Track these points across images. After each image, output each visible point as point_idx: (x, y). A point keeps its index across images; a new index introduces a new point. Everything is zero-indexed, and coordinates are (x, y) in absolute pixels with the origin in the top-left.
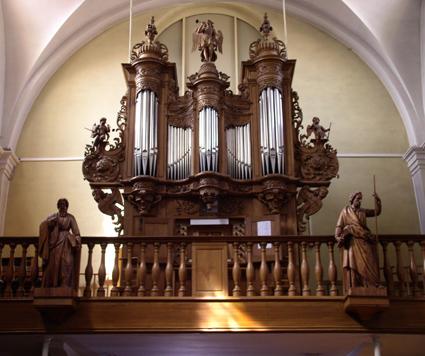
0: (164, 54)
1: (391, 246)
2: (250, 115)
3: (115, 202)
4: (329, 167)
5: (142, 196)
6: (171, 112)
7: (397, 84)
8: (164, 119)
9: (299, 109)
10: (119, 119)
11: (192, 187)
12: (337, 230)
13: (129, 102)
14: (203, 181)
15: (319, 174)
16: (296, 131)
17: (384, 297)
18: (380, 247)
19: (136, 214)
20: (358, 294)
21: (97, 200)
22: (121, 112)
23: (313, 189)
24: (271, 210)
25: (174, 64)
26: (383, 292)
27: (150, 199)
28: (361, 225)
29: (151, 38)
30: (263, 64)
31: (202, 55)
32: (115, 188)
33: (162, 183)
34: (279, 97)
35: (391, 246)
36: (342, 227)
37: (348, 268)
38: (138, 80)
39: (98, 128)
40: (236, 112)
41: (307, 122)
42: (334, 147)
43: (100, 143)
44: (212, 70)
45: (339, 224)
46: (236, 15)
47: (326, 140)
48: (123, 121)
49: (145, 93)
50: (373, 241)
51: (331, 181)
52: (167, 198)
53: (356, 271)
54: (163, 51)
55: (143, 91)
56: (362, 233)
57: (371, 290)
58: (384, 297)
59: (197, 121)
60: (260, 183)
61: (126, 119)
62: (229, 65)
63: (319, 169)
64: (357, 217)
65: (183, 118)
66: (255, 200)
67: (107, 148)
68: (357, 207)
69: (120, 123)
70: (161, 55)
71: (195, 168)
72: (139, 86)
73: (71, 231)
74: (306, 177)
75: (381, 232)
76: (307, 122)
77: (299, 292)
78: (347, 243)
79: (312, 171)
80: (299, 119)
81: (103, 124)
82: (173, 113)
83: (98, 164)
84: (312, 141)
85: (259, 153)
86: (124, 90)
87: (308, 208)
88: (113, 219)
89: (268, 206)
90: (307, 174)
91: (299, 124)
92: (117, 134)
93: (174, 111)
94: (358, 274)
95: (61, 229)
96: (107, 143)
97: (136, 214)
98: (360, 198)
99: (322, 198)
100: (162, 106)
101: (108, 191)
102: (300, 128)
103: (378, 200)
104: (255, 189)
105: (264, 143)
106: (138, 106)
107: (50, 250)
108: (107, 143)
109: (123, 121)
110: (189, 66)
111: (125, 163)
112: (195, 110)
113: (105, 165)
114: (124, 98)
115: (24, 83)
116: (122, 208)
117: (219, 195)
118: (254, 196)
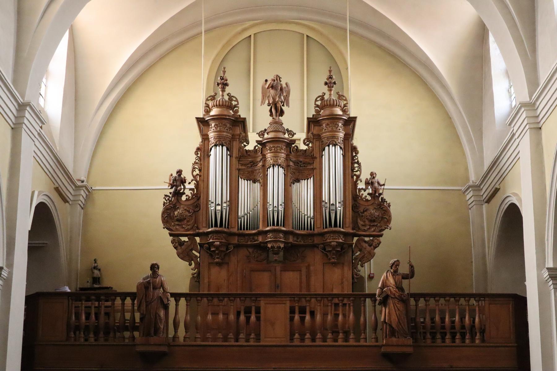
0: (235, 106)
2: (313, 169)
3: (192, 250)
4: (382, 218)
5: (217, 247)
6: (242, 165)
8: (235, 173)
9: (358, 163)
10: (194, 169)
11: (260, 239)
12: (378, 292)
13: (203, 153)
14: (270, 235)
15: (374, 226)
16: (355, 184)
17: (410, 346)
19: (211, 261)
21: (175, 248)
22: (195, 163)
23: (367, 239)
24: (330, 259)
25: (245, 119)
26: (410, 341)
27: (223, 249)
28: (397, 288)
29: (223, 90)
30: (327, 121)
31: (271, 111)
32: (191, 237)
33: (234, 234)
34: (339, 152)
36: (382, 288)
38: (212, 135)
39: (175, 180)
40: (303, 166)
41: (365, 175)
42: (388, 200)
43: (178, 194)
44: (277, 125)
45: (380, 285)
46: (306, 32)
47: (380, 194)
48: (197, 172)
49: (218, 147)
51: (384, 232)
52: (238, 246)
53: (390, 326)
54: (234, 103)
55: (216, 145)
56: (397, 294)
58: (410, 346)
59: (265, 176)
60: (322, 235)
61: (200, 170)
62: (296, 122)
63: (374, 221)
64: (394, 279)
65: (253, 172)
66: (316, 249)
67: (184, 198)
69: (195, 173)
70: (231, 107)
71: (263, 221)
72: (212, 141)
73: (161, 289)
74: (363, 228)
75: (412, 291)
76: (365, 175)
77: (324, 339)
78: (384, 302)
79: (367, 222)
80: (358, 173)
81: (180, 175)
82: (247, 166)
83: (176, 213)
84: (368, 194)
85: (321, 208)
86: (197, 141)
87: (363, 257)
88: (190, 265)
89: (327, 256)
90: (363, 225)
91: (358, 177)
92: (192, 186)
93: (245, 165)
95: (155, 288)
96: (184, 193)
97: (211, 261)
98: (398, 265)
99: (375, 248)
100: (234, 159)
101: (185, 239)
102: (359, 182)
103: (412, 267)
104: (317, 240)
105: (325, 197)
106: (212, 158)
107: (147, 306)
108: (184, 193)
109: (197, 172)
110: (258, 121)
111: (201, 211)
112: (263, 166)
113: (183, 210)
114: (198, 149)
115: (202, 188)
116: (198, 254)
117: (285, 247)
118: (314, 246)
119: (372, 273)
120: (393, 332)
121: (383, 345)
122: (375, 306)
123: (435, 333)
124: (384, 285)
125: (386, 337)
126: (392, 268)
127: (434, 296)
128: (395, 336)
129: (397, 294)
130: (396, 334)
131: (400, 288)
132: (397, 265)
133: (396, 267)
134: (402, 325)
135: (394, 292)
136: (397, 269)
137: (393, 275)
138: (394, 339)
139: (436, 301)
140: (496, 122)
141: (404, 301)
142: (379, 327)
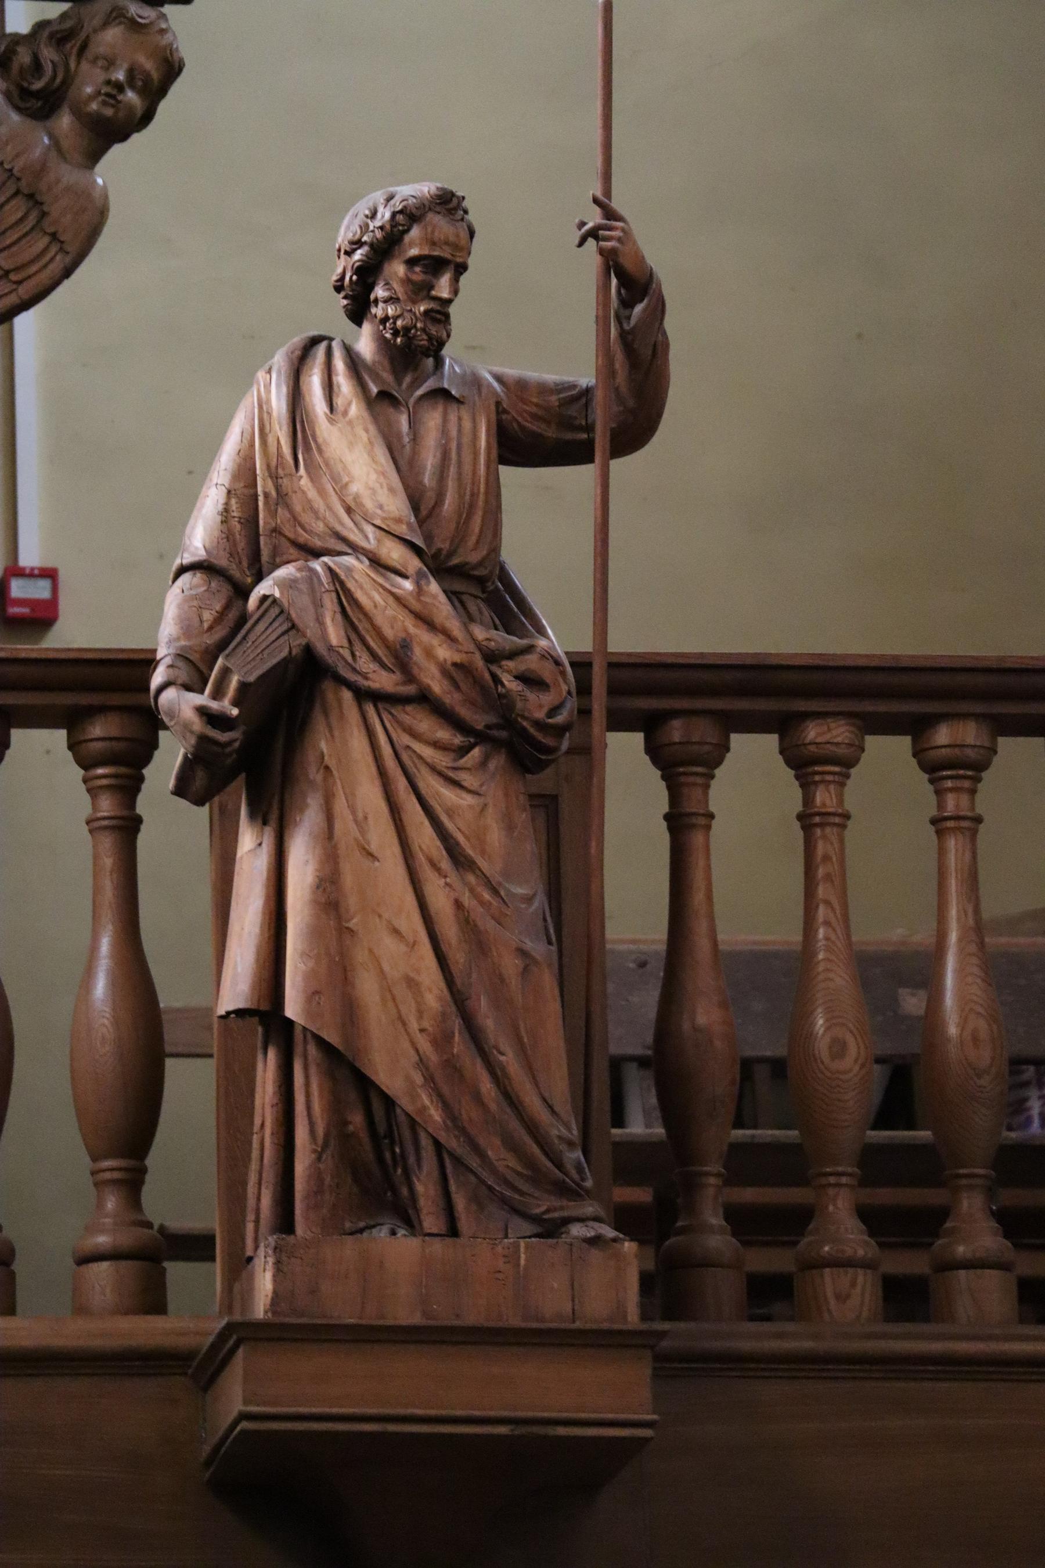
1: (751, 776)
7: (896, 1337)
12: (168, 621)
18: (627, 773)
20: (342, 1306)
26: (610, 1281)
28: (438, 565)
35: (751, 776)
36: (231, 572)
37: (266, 1015)
45: (199, 537)
50: (528, 735)
53: (346, 1070)
56: (434, 656)
57: (495, 1268)
64: (402, 458)
68: (414, 353)
75: (642, 631)
78: (258, 759)
94: (364, 1084)
98: (446, 263)
99: (108, 131)
103: (631, 285)
119: (29, 557)
120: (377, 1164)
121: (242, 1334)
122: (128, 827)
123: (929, 1166)
124: (253, 540)
125: (285, 1223)
126: (358, 311)
127: (899, 696)
128: (407, 1218)
129: (434, 656)
130: (425, 1188)
131: (481, 584)
132: (434, 265)
133: (421, 290)
134: (509, 1059)
135: (391, 621)
136: (440, 315)
137: (381, 402)
138: (396, 1250)
139: (933, 768)
140: (340, 1048)
141: (528, 735)
142: (189, 1089)
